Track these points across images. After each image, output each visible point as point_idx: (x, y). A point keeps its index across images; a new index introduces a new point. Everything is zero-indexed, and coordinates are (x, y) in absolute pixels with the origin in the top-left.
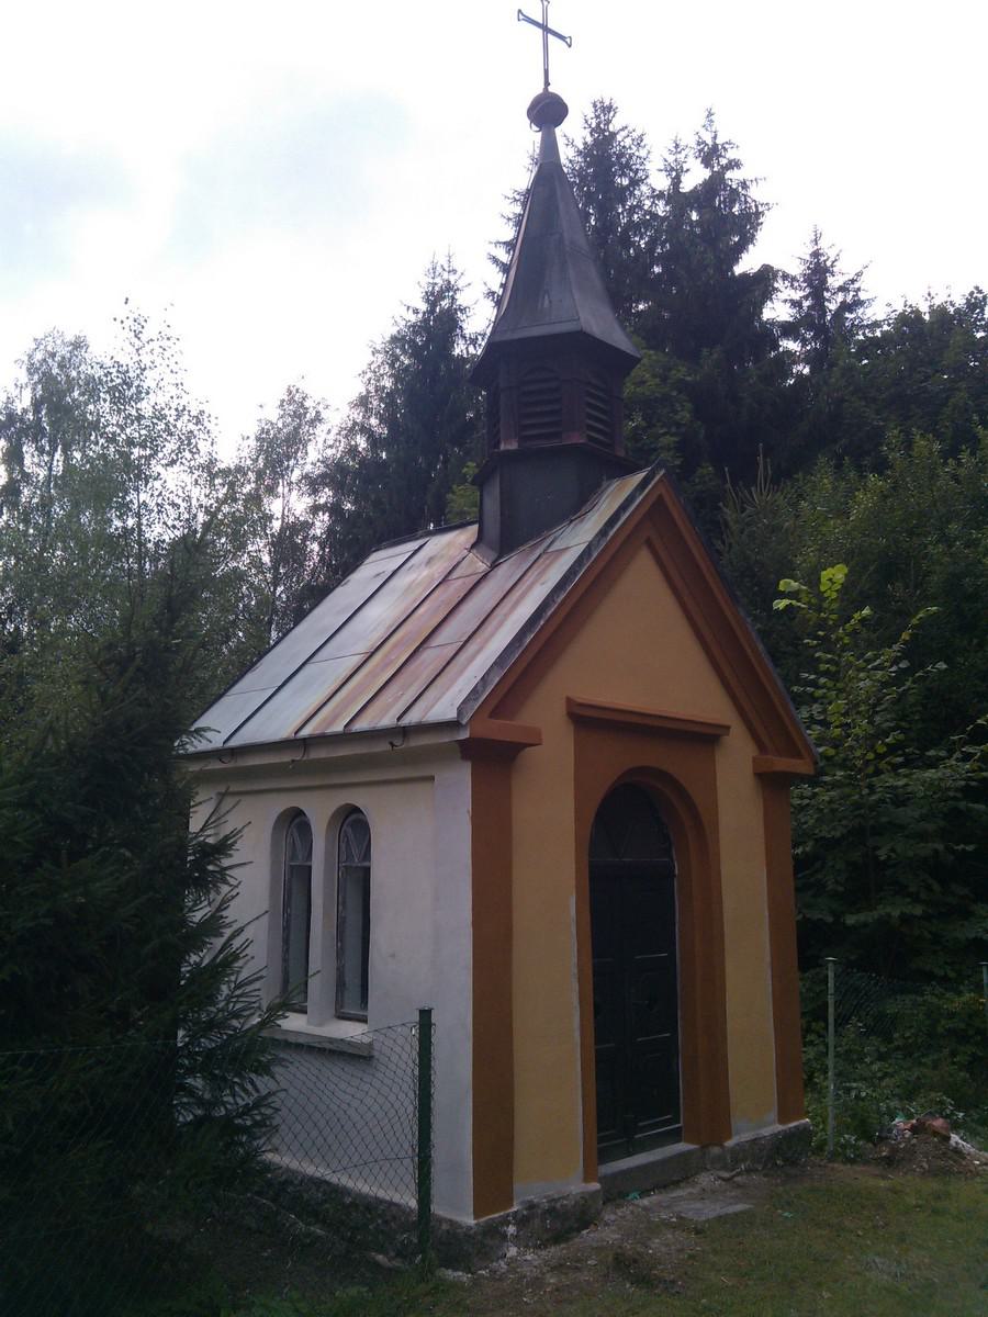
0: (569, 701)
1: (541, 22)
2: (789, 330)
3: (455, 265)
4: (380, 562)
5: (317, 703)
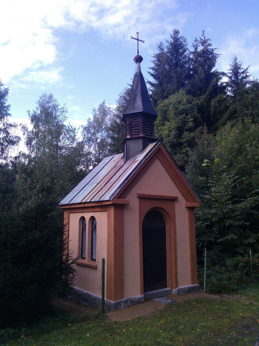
0: (137, 193)
4: (106, 160)
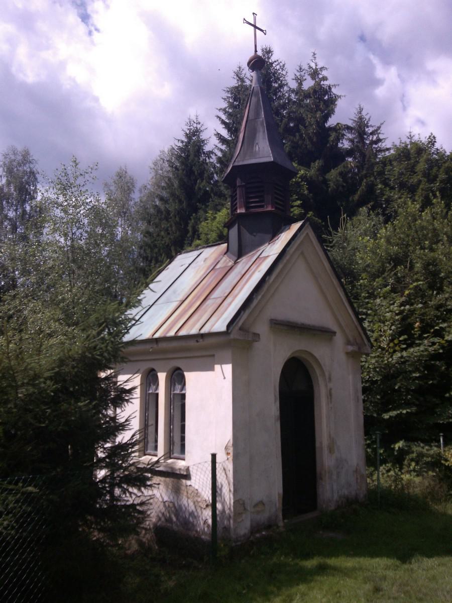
1: (257, 30)
2: (350, 153)
3: (199, 120)
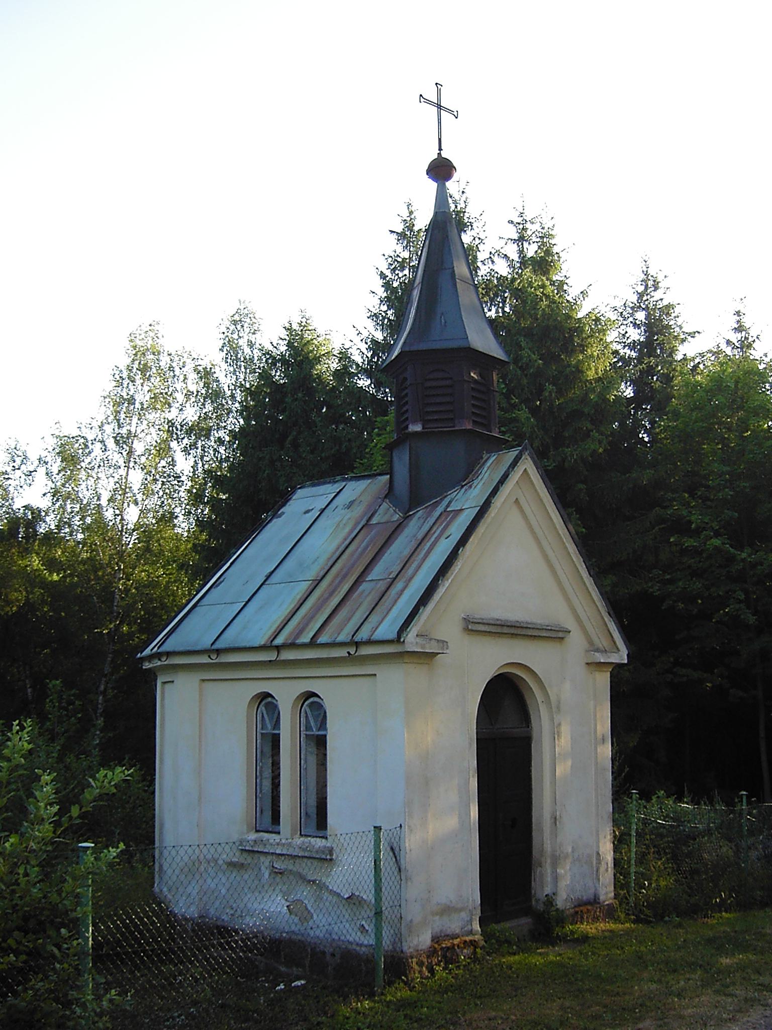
5: (282, 618)
